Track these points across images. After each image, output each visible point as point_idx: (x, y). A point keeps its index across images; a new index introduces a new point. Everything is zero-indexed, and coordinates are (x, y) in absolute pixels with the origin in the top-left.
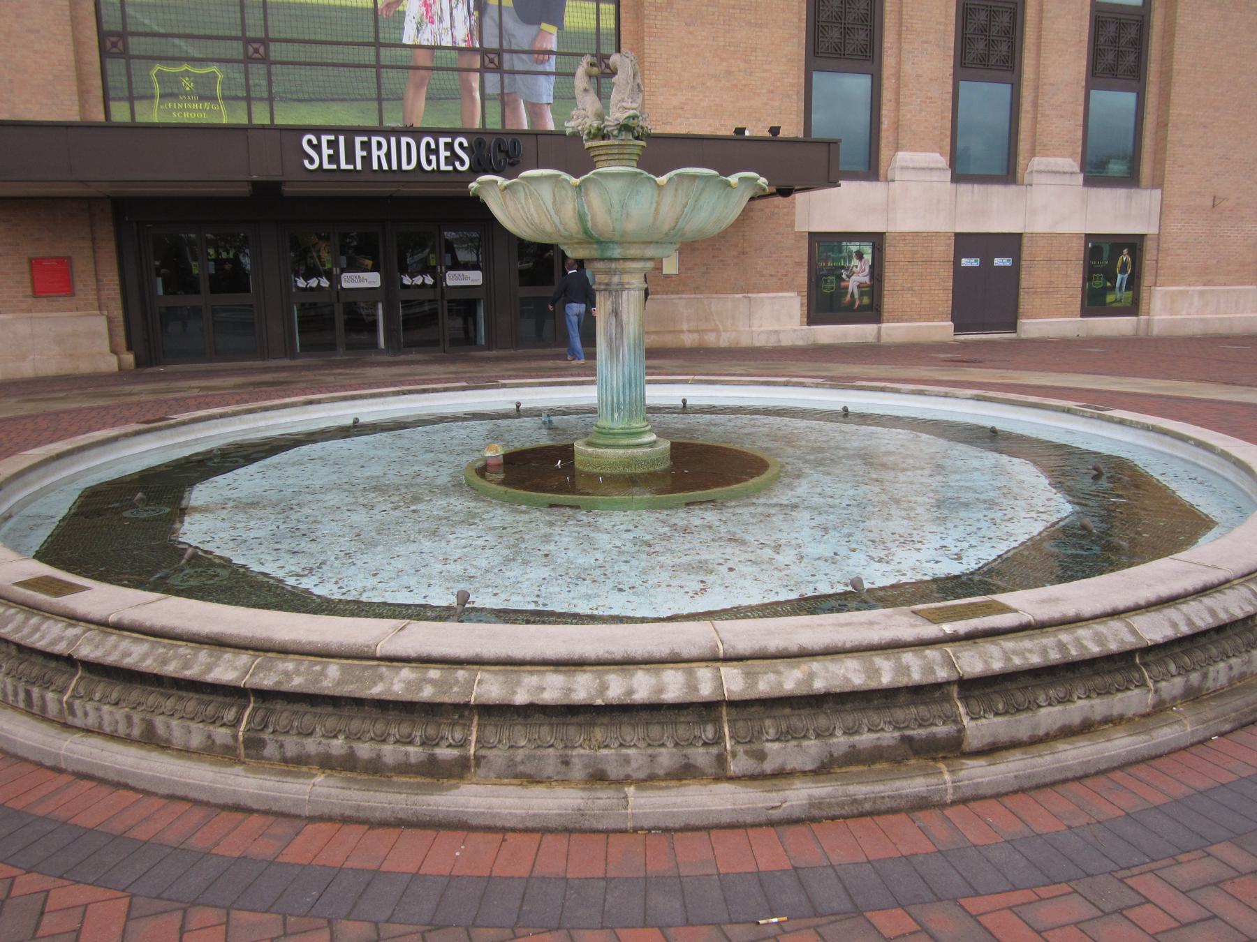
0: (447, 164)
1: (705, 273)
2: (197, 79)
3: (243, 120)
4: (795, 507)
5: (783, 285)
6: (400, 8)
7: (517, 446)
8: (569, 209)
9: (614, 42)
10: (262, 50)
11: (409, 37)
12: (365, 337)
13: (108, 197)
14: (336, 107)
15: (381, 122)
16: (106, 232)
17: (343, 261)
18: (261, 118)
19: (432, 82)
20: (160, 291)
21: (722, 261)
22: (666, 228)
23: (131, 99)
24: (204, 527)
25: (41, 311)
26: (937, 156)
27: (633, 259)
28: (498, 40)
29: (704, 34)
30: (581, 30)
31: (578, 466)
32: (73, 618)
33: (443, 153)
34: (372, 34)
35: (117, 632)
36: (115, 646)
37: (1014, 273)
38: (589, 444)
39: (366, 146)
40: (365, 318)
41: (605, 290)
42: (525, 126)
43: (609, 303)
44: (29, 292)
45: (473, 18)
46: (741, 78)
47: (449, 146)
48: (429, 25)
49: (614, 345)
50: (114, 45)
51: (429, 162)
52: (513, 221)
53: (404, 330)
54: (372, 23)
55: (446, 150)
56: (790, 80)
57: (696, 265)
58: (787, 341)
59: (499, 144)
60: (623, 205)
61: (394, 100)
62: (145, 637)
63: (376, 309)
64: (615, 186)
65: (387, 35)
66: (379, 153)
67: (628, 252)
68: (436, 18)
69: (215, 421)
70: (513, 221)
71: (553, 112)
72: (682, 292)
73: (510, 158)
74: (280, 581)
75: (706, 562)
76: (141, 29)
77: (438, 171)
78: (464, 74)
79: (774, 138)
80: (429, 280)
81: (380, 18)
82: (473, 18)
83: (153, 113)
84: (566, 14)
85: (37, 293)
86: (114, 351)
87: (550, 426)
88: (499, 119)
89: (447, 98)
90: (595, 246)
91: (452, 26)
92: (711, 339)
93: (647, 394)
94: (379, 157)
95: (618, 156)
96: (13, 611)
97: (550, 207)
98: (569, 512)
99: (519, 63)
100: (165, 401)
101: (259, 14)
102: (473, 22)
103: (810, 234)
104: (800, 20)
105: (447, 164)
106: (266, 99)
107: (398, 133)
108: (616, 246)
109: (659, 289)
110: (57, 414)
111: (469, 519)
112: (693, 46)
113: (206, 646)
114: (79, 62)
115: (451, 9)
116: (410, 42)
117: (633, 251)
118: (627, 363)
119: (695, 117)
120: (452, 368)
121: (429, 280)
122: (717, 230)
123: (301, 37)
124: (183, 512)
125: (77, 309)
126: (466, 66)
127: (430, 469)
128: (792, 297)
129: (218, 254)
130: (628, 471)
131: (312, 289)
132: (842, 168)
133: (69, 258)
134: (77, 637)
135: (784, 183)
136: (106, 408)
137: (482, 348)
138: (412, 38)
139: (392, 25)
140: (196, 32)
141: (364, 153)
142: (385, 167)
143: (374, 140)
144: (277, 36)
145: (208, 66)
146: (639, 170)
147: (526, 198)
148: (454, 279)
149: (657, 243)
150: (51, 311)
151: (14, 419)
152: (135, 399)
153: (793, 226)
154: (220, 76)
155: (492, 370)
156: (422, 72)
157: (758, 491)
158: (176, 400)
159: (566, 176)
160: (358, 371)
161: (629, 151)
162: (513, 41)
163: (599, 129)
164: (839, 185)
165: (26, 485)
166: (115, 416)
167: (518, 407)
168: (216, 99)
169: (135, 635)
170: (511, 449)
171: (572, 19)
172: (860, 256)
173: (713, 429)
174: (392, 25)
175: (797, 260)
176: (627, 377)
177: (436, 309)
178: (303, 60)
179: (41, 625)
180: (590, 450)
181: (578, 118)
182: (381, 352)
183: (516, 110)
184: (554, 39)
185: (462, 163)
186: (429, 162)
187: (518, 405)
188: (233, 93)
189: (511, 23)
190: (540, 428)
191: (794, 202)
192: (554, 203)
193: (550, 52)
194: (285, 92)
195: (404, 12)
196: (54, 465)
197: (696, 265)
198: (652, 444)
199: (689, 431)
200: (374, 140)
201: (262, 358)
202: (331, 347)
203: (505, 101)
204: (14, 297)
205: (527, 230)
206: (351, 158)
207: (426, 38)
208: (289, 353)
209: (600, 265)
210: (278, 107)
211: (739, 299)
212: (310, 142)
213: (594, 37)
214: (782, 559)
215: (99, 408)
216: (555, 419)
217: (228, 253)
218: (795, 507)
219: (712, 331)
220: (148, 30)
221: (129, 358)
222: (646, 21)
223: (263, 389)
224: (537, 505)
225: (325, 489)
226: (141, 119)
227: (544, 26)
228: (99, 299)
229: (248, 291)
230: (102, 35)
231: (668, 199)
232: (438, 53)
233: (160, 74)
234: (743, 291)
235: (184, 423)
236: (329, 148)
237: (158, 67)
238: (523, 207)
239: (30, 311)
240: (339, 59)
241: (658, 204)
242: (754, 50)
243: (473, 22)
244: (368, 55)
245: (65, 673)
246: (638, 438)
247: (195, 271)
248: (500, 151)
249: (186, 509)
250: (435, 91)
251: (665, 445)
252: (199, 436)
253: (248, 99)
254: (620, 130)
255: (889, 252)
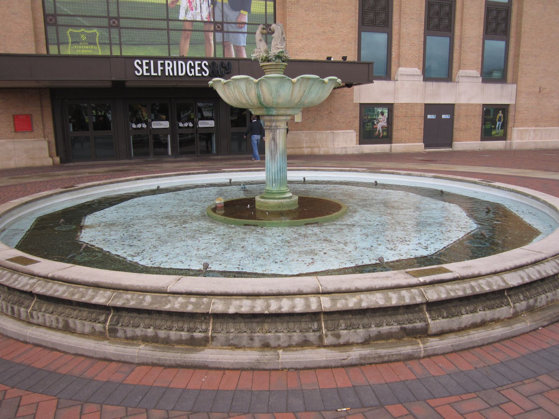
0: (199, 73)
1: (313, 121)
2: (87, 35)
3: (108, 53)
4: (353, 225)
5: (348, 127)
6: (178, 4)
7: (230, 198)
8: (253, 93)
9: (273, 19)
10: (116, 22)
11: (182, 17)
12: (162, 150)
13: (48, 88)
14: (149, 47)
15: (169, 54)
16: (47, 103)
17: (153, 116)
18: (116, 52)
19: (192, 36)
20: (71, 130)
21: (321, 116)
22: (296, 101)
23: (58, 44)
24: (91, 235)
25: (18, 138)
26: (417, 69)
27: (282, 115)
28: (221, 18)
29: (313, 15)
30: (258, 13)
31: (257, 207)
32: (33, 275)
33: (197, 68)
34: (166, 15)
35: (52, 281)
36: (51, 288)
37: (451, 122)
38: (262, 198)
39: (163, 65)
40: (162, 141)
41: (269, 129)
42: (234, 56)
43: (271, 135)
44: (13, 130)
45: (211, 8)
46: (329, 35)
47: (200, 65)
48: (191, 11)
49: (273, 153)
50: (51, 20)
51: (191, 72)
52: (228, 98)
53: (180, 147)
54: (165, 10)
55: (198, 67)
56: (351, 36)
57: (309, 118)
58: (350, 152)
59: (222, 64)
60: (277, 91)
61: (175, 44)
62: (65, 283)
63: (167, 137)
64: (273, 83)
65: (172, 16)
66: (169, 68)
67: (279, 112)
68: (194, 8)
69: (96, 187)
70: (228, 98)
71: (246, 50)
72: (303, 130)
73: (227, 70)
74: (125, 258)
75: (314, 250)
76: (63, 13)
77: (195, 76)
78: (207, 33)
79: (344, 61)
80: (191, 125)
81: (169, 8)
82: (211, 8)
83: (68, 50)
84: (252, 6)
85: (16, 130)
86: (51, 156)
87: (244, 190)
88: (222, 53)
89: (199, 44)
90: (265, 110)
91: (201, 12)
92: (316, 151)
93: (288, 175)
94: (168, 70)
95: (275, 69)
96: (6, 272)
97: (245, 92)
98: (253, 228)
99: (231, 28)
100: (74, 178)
101: (115, 6)
102: (210, 10)
103: (360, 104)
104: (356, 9)
105: (199, 73)
106: (118, 44)
107: (177, 59)
108: (274, 109)
109: (293, 128)
110: (25, 184)
111: (209, 231)
112: (308, 20)
113: (92, 288)
114: (35, 28)
115: (201, 4)
116: (182, 19)
117: (282, 112)
118: (279, 161)
119: (309, 52)
120: (201, 164)
121: (191, 125)
122: (319, 103)
123: (134, 17)
124: (81, 228)
125: (34, 138)
126: (207, 29)
127: (191, 209)
128: (352, 132)
129: (97, 113)
130: (279, 209)
131: (139, 128)
132: (374, 75)
133: (31, 115)
134: (34, 284)
135: (349, 81)
136: (47, 181)
137: (214, 155)
138: (183, 17)
139: (174, 11)
140: (87, 14)
141: (162, 68)
142: (171, 74)
143: (167, 62)
144: (123, 16)
145: (92, 29)
146: (284, 76)
147: (234, 88)
148: (202, 124)
149: (292, 108)
150: (23, 138)
151: (6, 186)
152: (60, 177)
153: (353, 100)
154: (98, 34)
155: (219, 165)
156: (188, 32)
157: (337, 218)
158: (78, 178)
159: (252, 78)
160: (159, 165)
161: (280, 67)
162: (228, 18)
163: (266, 58)
164: (373, 82)
165: (11, 216)
166: (51, 185)
167: (230, 181)
168: (96, 44)
169: (60, 282)
170: (227, 200)
171: (254, 9)
172: (382, 114)
173: (317, 191)
174: (174, 11)
175: (355, 116)
176: (279, 168)
177: (194, 137)
178: (135, 27)
179: (18, 278)
180: (262, 200)
181: (257, 53)
182: (169, 157)
183: (229, 49)
184: (247, 17)
185: (206, 73)
186: (191, 72)
187: (230, 180)
188: (104, 41)
189: (227, 10)
190: (240, 190)
191: (353, 90)
192: (246, 90)
193: (245, 23)
194: (127, 41)
195: (180, 6)
196: (24, 207)
197: (309, 118)
198: (290, 198)
199: (306, 191)
200: (167, 62)
201: (117, 159)
202: (147, 154)
203: (225, 45)
204: (6, 132)
205: (234, 102)
206: (156, 70)
207: (189, 17)
208: (129, 157)
209: (267, 118)
210: (123, 47)
211: (329, 133)
212: (138, 63)
213: (264, 16)
214: (348, 249)
215: (44, 181)
216: (247, 186)
217: (101, 113)
218: (353, 225)
219: (317, 147)
220: (66, 13)
221: (57, 159)
222: (287, 9)
223: (117, 173)
224: (239, 225)
225: (145, 218)
226: (63, 53)
227: (242, 12)
228: (44, 133)
229: (110, 129)
230: (45, 16)
231: (297, 88)
232: (195, 23)
233: (71, 33)
234: (330, 129)
235: (82, 188)
236: (146, 66)
237: (70, 30)
238: (232, 92)
239: (13, 138)
240: (151, 26)
241: (293, 91)
242: (335, 22)
243: (210, 10)
244: (164, 24)
245: (29, 299)
246: (284, 195)
247: (87, 121)
248: (223, 67)
249: (83, 226)
250: (193, 41)
251: (296, 198)
252: (88, 194)
253: (110, 44)
254: (276, 58)
255: (396, 112)
